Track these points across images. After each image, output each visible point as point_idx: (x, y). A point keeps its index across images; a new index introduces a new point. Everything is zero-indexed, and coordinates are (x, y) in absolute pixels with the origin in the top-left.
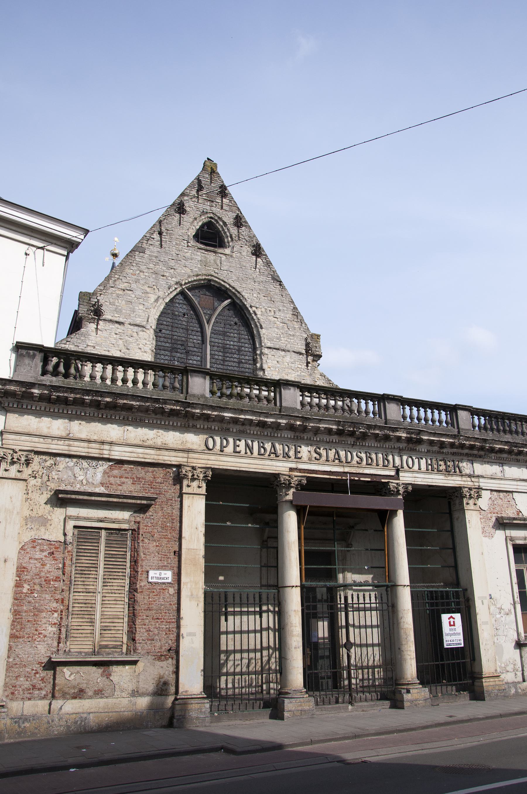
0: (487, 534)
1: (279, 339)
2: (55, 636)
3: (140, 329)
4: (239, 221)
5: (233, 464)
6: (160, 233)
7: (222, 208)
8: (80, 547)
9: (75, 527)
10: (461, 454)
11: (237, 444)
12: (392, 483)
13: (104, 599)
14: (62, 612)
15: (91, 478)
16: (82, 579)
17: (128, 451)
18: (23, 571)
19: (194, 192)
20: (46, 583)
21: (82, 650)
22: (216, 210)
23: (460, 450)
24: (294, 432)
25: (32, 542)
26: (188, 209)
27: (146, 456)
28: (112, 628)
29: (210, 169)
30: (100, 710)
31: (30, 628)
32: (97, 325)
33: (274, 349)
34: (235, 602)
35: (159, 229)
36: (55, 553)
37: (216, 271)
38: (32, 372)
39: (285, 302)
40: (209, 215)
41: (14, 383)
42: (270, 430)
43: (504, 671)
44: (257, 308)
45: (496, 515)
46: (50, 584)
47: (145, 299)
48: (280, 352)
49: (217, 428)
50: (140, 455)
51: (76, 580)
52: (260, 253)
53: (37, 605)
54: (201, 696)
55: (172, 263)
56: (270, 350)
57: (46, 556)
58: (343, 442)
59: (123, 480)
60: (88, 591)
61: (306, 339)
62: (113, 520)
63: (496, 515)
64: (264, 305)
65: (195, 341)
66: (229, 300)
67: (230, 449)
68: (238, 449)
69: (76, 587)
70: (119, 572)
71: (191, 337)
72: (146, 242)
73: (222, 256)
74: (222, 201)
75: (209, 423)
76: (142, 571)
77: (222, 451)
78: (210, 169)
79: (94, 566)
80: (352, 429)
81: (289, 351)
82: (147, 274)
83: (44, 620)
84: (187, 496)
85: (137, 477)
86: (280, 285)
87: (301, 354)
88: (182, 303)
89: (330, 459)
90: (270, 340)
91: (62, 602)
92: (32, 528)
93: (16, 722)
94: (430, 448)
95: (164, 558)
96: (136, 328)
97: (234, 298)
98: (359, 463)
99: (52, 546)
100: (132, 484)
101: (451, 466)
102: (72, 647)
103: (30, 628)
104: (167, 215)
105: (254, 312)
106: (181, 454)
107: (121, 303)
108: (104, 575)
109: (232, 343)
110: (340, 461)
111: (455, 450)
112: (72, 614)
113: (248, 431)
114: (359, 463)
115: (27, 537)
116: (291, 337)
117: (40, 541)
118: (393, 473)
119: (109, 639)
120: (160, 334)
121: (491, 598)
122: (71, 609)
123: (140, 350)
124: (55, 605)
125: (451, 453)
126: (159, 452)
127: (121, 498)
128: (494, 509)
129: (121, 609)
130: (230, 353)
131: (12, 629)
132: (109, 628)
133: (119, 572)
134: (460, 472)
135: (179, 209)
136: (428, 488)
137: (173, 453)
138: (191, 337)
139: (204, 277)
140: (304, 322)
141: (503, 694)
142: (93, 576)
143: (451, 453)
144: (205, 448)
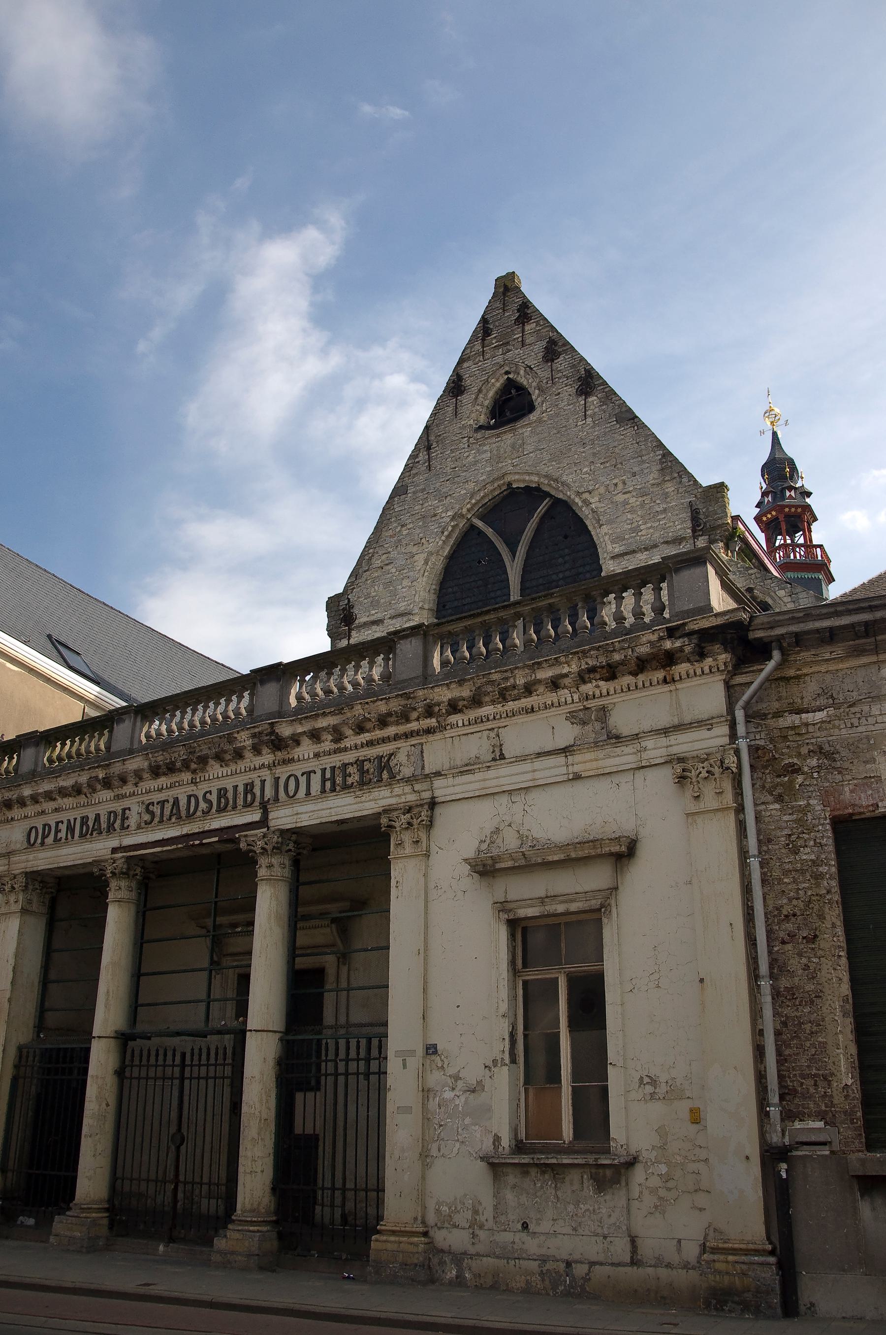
12: (246, 836)
19: (478, 347)
29: (506, 287)
64: (602, 479)
67: (50, 840)
71: (492, 595)
77: (43, 844)
78: (506, 287)
82: (411, 526)
97: (553, 493)
110: (179, 817)
111: (366, 737)
118: (256, 817)
134: (392, 776)
143: (362, 744)
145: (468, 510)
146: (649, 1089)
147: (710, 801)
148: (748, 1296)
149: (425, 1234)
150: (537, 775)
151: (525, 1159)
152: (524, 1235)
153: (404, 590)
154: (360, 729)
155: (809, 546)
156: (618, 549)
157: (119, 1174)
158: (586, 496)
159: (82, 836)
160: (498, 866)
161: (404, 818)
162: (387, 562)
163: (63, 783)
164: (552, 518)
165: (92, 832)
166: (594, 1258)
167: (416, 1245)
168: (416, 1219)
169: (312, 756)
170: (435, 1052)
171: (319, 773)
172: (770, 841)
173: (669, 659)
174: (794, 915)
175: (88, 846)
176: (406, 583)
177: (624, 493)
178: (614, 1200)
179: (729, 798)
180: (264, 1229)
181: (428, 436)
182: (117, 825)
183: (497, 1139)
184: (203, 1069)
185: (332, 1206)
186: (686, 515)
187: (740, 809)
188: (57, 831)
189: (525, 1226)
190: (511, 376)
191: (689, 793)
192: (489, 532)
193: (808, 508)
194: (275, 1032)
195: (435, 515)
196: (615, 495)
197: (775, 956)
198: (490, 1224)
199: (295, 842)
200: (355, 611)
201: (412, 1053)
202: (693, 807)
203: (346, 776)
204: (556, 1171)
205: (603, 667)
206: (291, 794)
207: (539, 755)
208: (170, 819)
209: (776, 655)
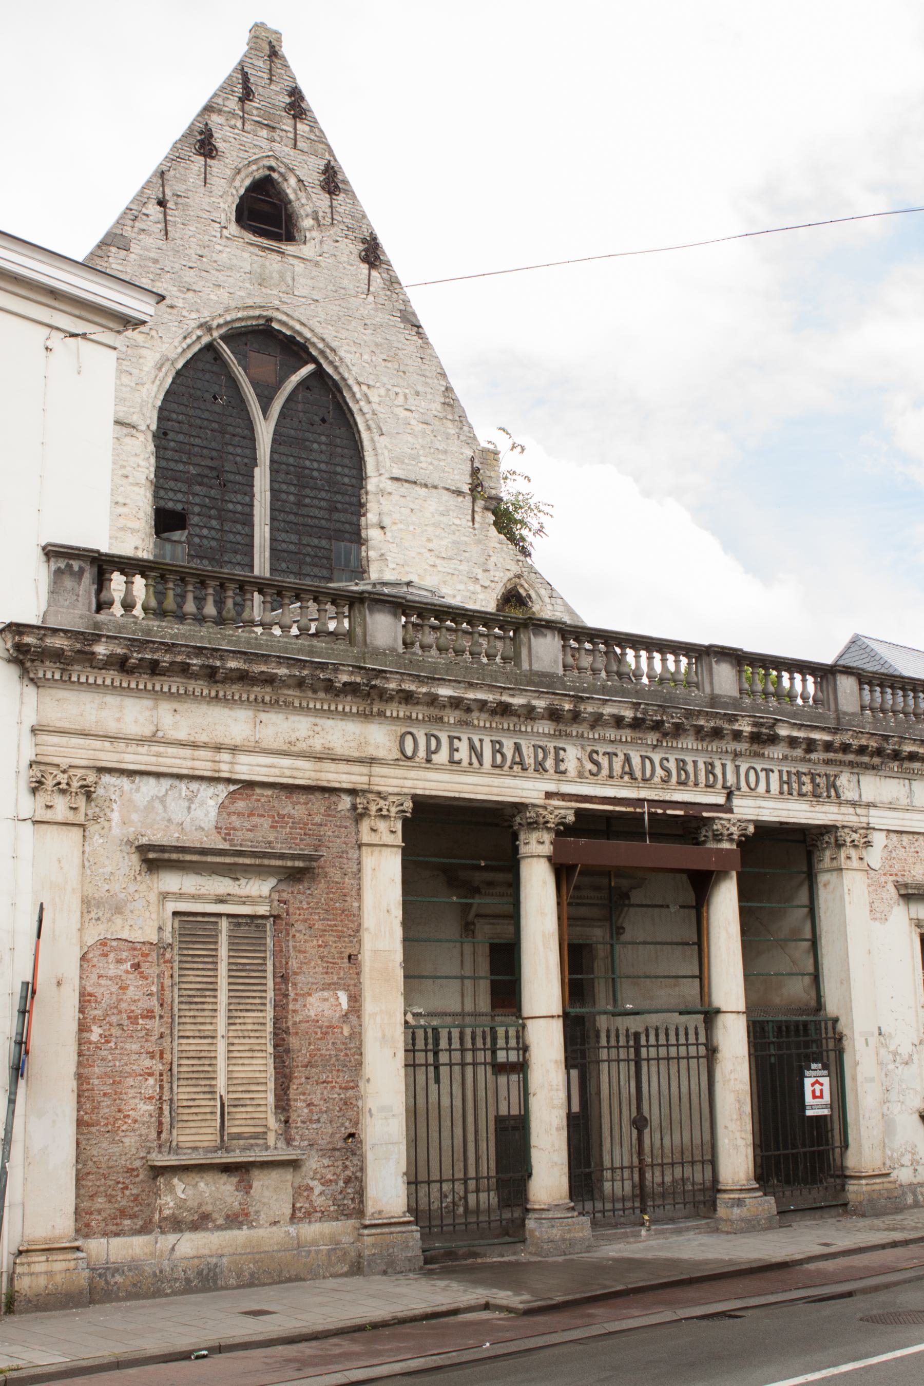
0: (878, 915)
2: (154, 1119)
3: (125, 430)
4: (332, 181)
5: (449, 786)
6: (162, 203)
8: (185, 952)
9: (175, 914)
10: (841, 763)
11: (455, 747)
12: (720, 819)
13: (231, 1048)
14: (161, 1075)
15: (196, 816)
16: (192, 1013)
17: (263, 764)
18: (89, 1001)
19: (233, 104)
20: (131, 1023)
21: (198, 1144)
22: (284, 150)
23: (840, 755)
24: (555, 724)
25: (101, 944)
26: (220, 145)
27: (296, 774)
28: (248, 1102)
30: (239, 1250)
31: (108, 1106)
33: (406, 481)
34: (453, 1047)
35: (160, 195)
36: (142, 964)
37: (285, 298)
38: (80, 605)
39: (427, 374)
40: (267, 163)
41: (62, 635)
42: (515, 719)
43: (896, 1166)
44: (369, 386)
45: (894, 878)
46: (138, 1024)
47: (134, 360)
48: (418, 488)
49: (420, 717)
50: (286, 771)
51: (182, 1014)
52: (377, 258)
53: (117, 1063)
54: (405, 1219)
55: (189, 277)
56: (397, 484)
57: (127, 972)
58: (639, 742)
59: (256, 820)
60: (202, 1034)
61: (472, 460)
62: (244, 899)
63: (894, 878)
64: (385, 380)
65: (238, 459)
67: (442, 757)
68: (457, 756)
69: (181, 1027)
70: (254, 997)
71: (231, 449)
72: (130, 223)
73: (295, 262)
74: (295, 129)
75: (409, 706)
76: (296, 994)
77: (429, 761)
78: (268, 48)
79: (211, 987)
80: (659, 718)
81: (435, 487)
83: (132, 1092)
84: (369, 849)
85: (278, 814)
86: (418, 333)
87: (459, 493)
89: (615, 774)
90: (398, 460)
91: (161, 1058)
92: (98, 919)
93: (100, 1275)
95: (332, 968)
97: (322, 361)
98: (665, 781)
99: (136, 953)
100: (272, 827)
101: (822, 785)
102: (181, 1138)
103: (108, 1106)
104: (175, 157)
105: (366, 396)
106: (356, 768)
108: (230, 1004)
109: (315, 465)
110: (633, 778)
111: (831, 755)
112: (179, 1079)
113: (476, 722)
114: (665, 781)
115: (93, 935)
117: (114, 943)
118: (721, 800)
119: (243, 1122)
121: (880, 1034)
122: (175, 1069)
123: (125, 481)
124: (148, 1063)
125: (824, 760)
126: (319, 765)
127: (259, 857)
128: (891, 867)
129: (263, 1067)
130: (312, 489)
131: (78, 1111)
132: (241, 1102)
133: (254, 997)
134: (838, 796)
135: (202, 142)
136: (778, 825)
137: (343, 767)
138: (231, 449)
140: (467, 422)
141: (892, 1202)
142: (210, 1007)
143: (824, 760)
144: (399, 756)
145: (219, 326)
177: (406, 409)
181: (163, 186)
184: (683, 1050)
186: (467, 468)
188: (453, 750)
190: (275, 175)
202: (42, 815)
208: (622, 778)
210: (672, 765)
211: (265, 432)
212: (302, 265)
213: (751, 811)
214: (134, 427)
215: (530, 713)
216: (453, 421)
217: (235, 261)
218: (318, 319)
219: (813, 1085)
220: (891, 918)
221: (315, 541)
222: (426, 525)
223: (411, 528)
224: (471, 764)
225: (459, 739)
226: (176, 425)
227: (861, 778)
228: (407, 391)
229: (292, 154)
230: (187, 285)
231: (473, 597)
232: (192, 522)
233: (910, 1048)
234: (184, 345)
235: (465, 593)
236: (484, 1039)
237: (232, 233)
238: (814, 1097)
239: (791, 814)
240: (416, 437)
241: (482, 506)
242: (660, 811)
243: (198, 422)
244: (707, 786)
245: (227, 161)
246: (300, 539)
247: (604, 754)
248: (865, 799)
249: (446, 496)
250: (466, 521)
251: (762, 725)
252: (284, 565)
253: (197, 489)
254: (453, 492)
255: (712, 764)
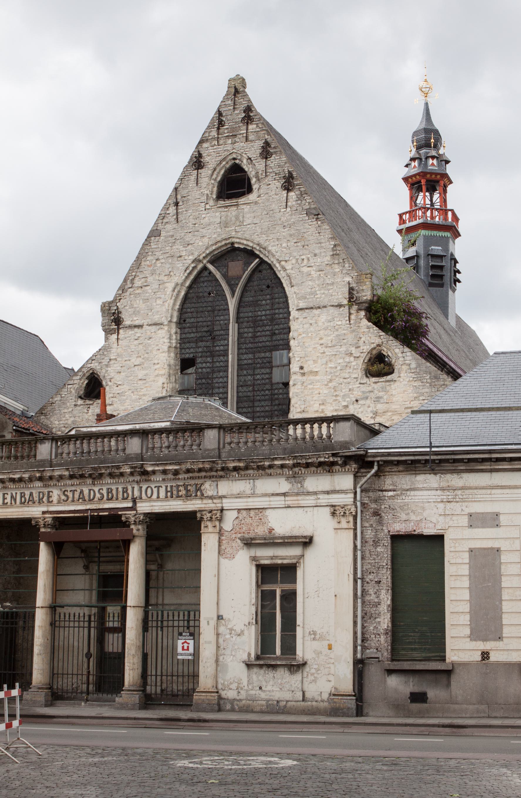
1: (314, 294)
3: (158, 327)
6: (177, 204)
7: (247, 139)
10: (205, 477)
12: (125, 514)
19: (214, 133)
29: (237, 89)
32: (118, 335)
33: (307, 309)
35: (176, 201)
40: (231, 157)
44: (286, 261)
55: (189, 238)
56: (301, 312)
61: (349, 283)
66: (257, 260)
68: (6, 501)
71: (218, 318)
73: (244, 206)
81: (325, 307)
82: (163, 261)
87: (340, 306)
88: (206, 281)
94: (164, 477)
96: (154, 327)
97: (262, 256)
101: (192, 490)
107: (139, 304)
109: (264, 313)
113: (10, 486)
116: (330, 287)
118: (130, 505)
120: (184, 325)
123: (158, 351)
125: (188, 478)
134: (203, 495)
138: (218, 318)
139: (223, 243)
145: (204, 258)
146: (313, 636)
147: (344, 524)
148: (345, 710)
149: (217, 692)
150: (272, 503)
151: (261, 662)
152: (260, 692)
153: (158, 306)
154: (188, 471)
155: (444, 211)
156: (302, 305)
157: (55, 672)
158: (283, 263)
159: (21, 503)
160: (253, 542)
161: (209, 515)
162: (145, 284)
163: (12, 476)
164: (260, 271)
165: (29, 501)
166: (288, 699)
167: (214, 696)
168: (213, 686)
169: (161, 479)
170: (222, 619)
171: (164, 488)
172: (366, 542)
173: (333, 464)
174: (373, 573)
175: (26, 509)
176: (159, 302)
177: (308, 267)
178: (298, 677)
179: (351, 525)
180: (140, 693)
181: (176, 195)
182: (45, 499)
183: (249, 654)
185: (156, 686)
186: (346, 290)
187: (355, 529)
189: (260, 688)
190: (237, 162)
191: (336, 520)
192: (218, 275)
193: (445, 176)
194: (142, 607)
195: (180, 257)
196: (303, 267)
197: (364, 588)
198: (246, 688)
199: (149, 518)
200: (122, 316)
201: (212, 619)
202: (337, 526)
203: (178, 491)
204: (274, 667)
205: (304, 464)
206: (149, 496)
207: (273, 495)
208: (78, 501)
209: (376, 468)
210: (104, 492)
211: (232, 304)
212: (248, 207)
213: (148, 508)
214: (161, 324)
215: (31, 480)
216: (338, 263)
217: (212, 220)
218: (257, 234)
219: (183, 643)
220: (237, 557)
221: (263, 355)
222: (319, 331)
223: (310, 335)
224: (11, 503)
225: (7, 494)
226: (190, 314)
227: (219, 483)
228: (309, 256)
229: (245, 145)
230: (187, 243)
231: (349, 365)
232: (198, 362)
233: (243, 627)
234: (186, 274)
235: (343, 364)
236: (95, 617)
237: (211, 205)
238: (183, 649)
239: (172, 507)
240: (314, 281)
241: (356, 309)
242: (96, 514)
243: (201, 309)
244: (123, 499)
245: (209, 166)
246: (254, 356)
247: (71, 491)
248: (220, 494)
249: (332, 310)
250: (345, 321)
251: (136, 467)
252: (245, 372)
253: (200, 344)
254: (336, 306)
255: (127, 489)
